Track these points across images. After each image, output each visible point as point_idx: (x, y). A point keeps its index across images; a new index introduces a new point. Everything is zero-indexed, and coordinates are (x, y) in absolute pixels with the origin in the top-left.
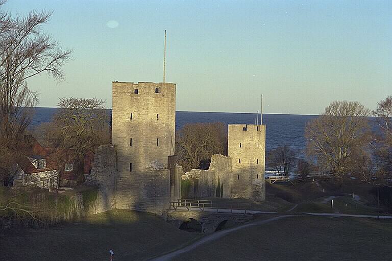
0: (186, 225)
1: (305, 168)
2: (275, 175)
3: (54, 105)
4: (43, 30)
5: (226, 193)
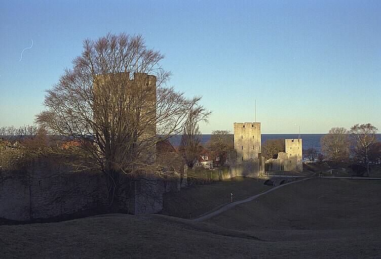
0: (267, 182)
1: (321, 157)
2: (307, 161)
3: (327, 132)
4: (199, 104)
5: (286, 169)
